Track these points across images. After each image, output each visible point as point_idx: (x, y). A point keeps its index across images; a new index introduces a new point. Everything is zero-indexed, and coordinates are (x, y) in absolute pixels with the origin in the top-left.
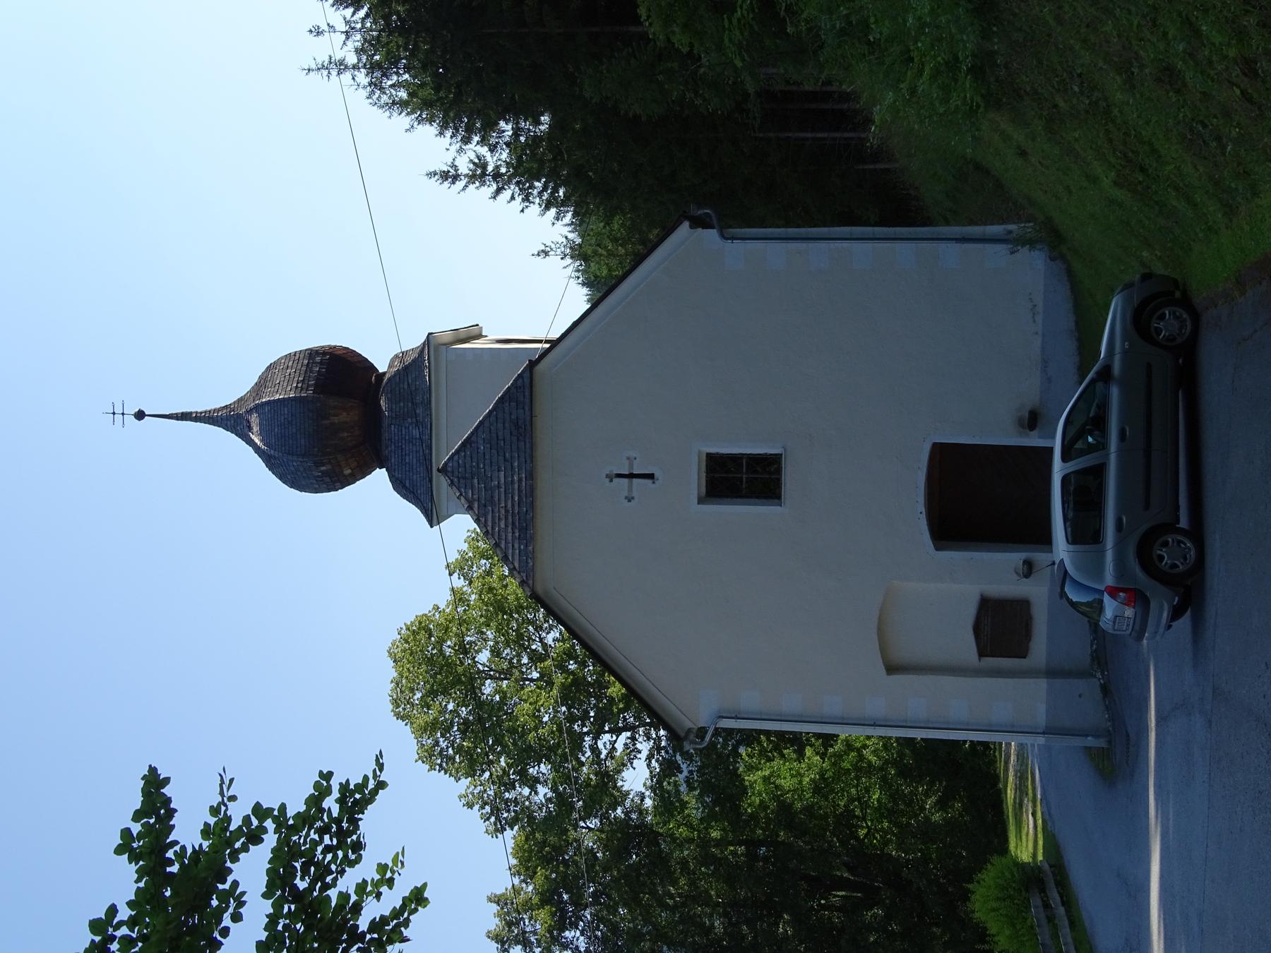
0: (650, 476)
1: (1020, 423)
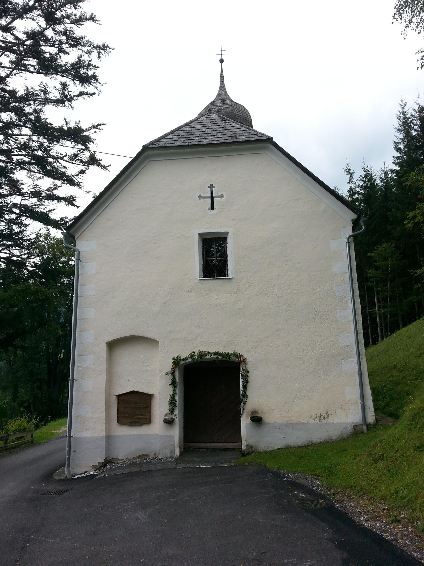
0: (212, 208)
1: (255, 412)
